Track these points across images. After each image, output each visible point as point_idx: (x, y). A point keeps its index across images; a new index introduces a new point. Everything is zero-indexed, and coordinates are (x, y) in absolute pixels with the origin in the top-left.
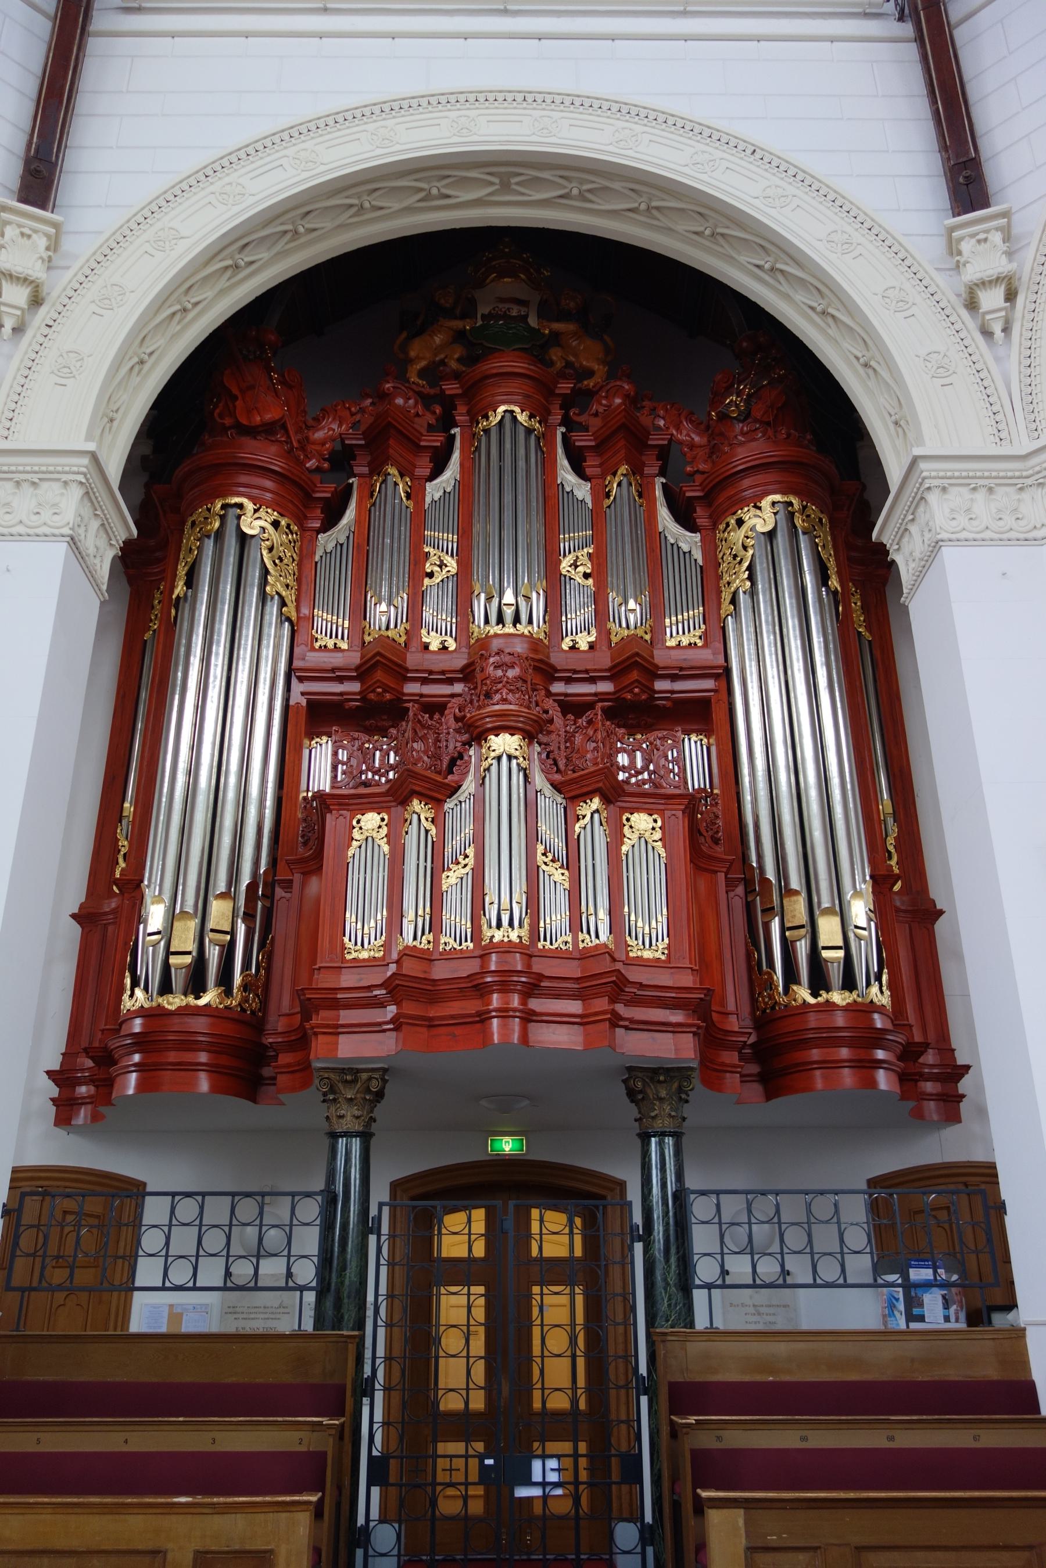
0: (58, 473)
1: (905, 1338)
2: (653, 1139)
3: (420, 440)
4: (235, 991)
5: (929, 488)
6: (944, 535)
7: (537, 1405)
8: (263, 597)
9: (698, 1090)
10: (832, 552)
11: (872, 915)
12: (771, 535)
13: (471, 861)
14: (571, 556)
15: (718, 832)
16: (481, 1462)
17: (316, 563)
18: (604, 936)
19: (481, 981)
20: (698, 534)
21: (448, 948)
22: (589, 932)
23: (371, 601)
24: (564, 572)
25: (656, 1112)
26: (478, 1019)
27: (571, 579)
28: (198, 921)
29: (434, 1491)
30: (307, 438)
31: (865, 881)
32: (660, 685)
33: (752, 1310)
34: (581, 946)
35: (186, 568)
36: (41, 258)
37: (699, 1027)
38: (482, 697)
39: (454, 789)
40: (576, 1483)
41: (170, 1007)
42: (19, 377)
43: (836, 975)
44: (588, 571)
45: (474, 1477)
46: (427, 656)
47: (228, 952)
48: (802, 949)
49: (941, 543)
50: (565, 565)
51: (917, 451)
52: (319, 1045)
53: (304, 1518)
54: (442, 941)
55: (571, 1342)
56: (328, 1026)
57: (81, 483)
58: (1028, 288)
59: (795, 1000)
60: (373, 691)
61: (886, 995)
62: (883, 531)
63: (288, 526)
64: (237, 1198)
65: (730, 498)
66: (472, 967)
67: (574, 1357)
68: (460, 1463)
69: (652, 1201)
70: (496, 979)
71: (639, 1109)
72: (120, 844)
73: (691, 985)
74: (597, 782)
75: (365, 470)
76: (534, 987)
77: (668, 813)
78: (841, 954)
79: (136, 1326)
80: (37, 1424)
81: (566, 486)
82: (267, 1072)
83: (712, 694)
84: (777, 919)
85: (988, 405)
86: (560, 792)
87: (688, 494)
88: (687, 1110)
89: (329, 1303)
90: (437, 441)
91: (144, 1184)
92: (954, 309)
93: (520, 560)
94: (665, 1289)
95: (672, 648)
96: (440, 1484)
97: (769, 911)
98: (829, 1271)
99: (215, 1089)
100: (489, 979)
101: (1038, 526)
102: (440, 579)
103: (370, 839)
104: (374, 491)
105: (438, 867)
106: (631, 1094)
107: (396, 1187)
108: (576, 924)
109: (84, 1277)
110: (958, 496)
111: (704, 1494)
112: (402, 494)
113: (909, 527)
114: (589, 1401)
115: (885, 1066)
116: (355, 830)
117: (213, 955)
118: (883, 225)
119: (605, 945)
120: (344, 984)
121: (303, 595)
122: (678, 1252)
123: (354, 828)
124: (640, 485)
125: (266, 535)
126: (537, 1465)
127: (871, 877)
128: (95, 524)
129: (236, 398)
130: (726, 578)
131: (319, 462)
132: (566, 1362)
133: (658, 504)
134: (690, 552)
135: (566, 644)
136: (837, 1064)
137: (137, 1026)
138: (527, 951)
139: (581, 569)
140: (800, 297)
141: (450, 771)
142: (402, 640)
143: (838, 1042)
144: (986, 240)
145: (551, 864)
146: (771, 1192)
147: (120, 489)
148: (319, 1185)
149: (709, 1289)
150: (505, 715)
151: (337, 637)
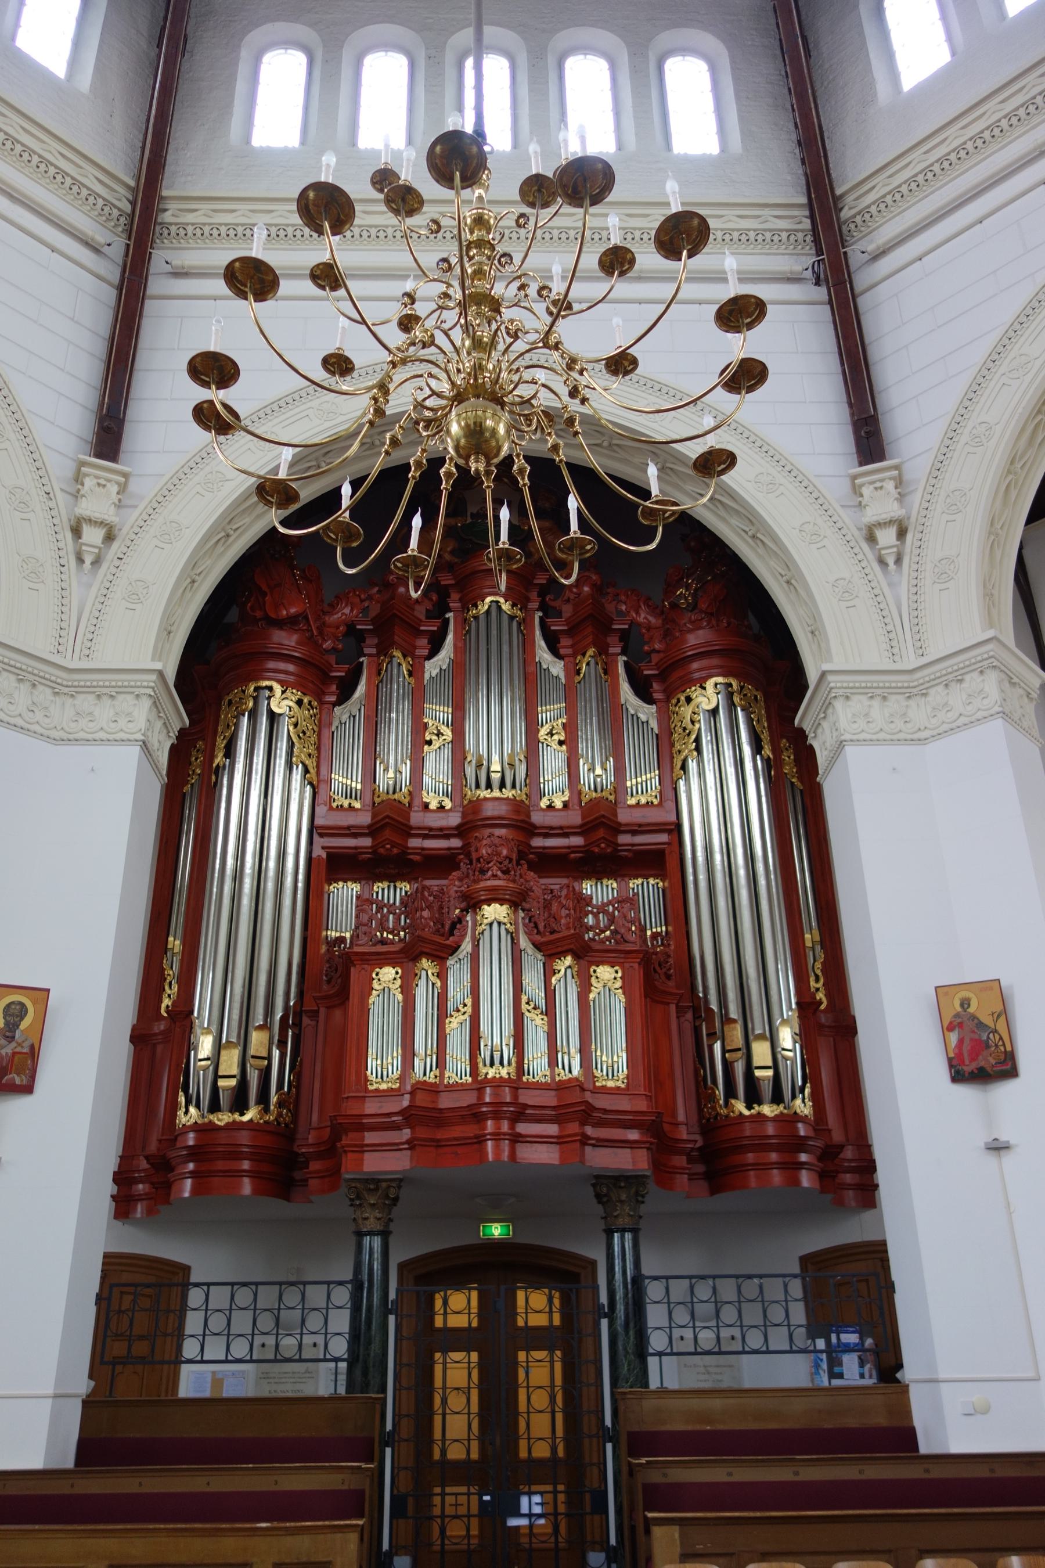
0: (132, 687)
1: (812, 1394)
2: (616, 1234)
3: (420, 626)
4: (272, 1107)
5: (835, 697)
6: (847, 737)
7: (523, 1454)
8: (290, 765)
9: (652, 1187)
10: (766, 725)
11: (797, 1038)
12: (714, 712)
13: (469, 1009)
14: (547, 726)
15: (670, 969)
16: (481, 1498)
17: (333, 733)
18: (576, 1071)
19: (478, 1111)
20: (654, 706)
21: (451, 1082)
22: (563, 1068)
23: (379, 769)
24: (541, 739)
25: (618, 1212)
26: (475, 1140)
27: (548, 746)
28: (240, 1048)
29: (443, 1522)
30: (324, 623)
31: (790, 1008)
32: (624, 839)
33: (702, 1370)
34: (557, 1079)
35: (225, 742)
36: (114, 503)
37: (651, 1143)
38: (477, 873)
39: (454, 949)
40: (556, 1514)
41: (219, 1123)
42: (97, 603)
43: (767, 1090)
44: (562, 738)
45: (474, 1510)
46: (428, 815)
47: (265, 1074)
48: (739, 1068)
49: (844, 743)
50: (543, 732)
51: (826, 667)
52: (348, 1161)
53: (353, 1537)
54: (446, 1076)
55: (551, 1401)
56: (355, 1146)
57: (150, 695)
58: (915, 528)
59: (733, 1112)
60: (383, 847)
61: (808, 1106)
62: (804, 718)
63: (310, 703)
64: (283, 1287)
65: (680, 678)
66: (470, 1099)
67: (553, 1413)
68: (463, 1499)
69: (614, 1285)
70: (490, 1109)
71: (605, 1209)
72: (166, 973)
73: (645, 1109)
74: (571, 944)
75: (374, 651)
76: (520, 1114)
77: (627, 965)
78: (770, 1073)
79: (185, 1391)
80: (138, 1471)
81: (543, 664)
82: (298, 1175)
83: (666, 846)
84: (719, 1042)
85: (883, 625)
86: (540, 950)
87: (646, 672)
88: (643, 1209)
89: (358, 1372)
90: (434, 626)
91: (186, 1269)
92: (857, 542)
93: (504, 681)
94: (625, 1356)
95: (631, 806)
96: (448, 1516)
97: (712, 1035)
98: (755, 1340)
99: (256, 1191)
100: (484, 1109)
101: (922, 728)
102: (438, 745)
103: (386, 989)
104: (381, 670)
105: (443, 1014)
106: (598, 1197)
107: (402, 1267)
108: (553, 1062)
109: (141, 1348)
110: (858, 703)
111: (650, 1515)
112: (405, 672)
113: (821, 722)
114: (567, 1448)
115: (806, 1167)
116: (375, 981)
117: (253, 1077)
118: (801, 469)
119: (576, 1079)
120: (368, 1111)
121: (322, 761)
122: (635, 1327)
123: (373, 979)
124: (606, 663)
125: (291, 713)
126: (524, 1501)
127: (797, 1003)
128: (159, 724)
129: (266, 594)
130: (677, 746)
131: (334, 642)
132: (547, 1417)
133: (621, 679)
134: (647, 722)
135: (544, 803)
136: (767, 1166)
137: (191, 1139)
138: (516, 1083)
139: (556, 737)
140: (734, 521)
141: (452, 934)
142: (406, 801)
143: (770, 1148)
144: (881, 488)
145: (533, 1011)
146: (710, 1277)
147: (175, 686)
148: (349, 1276)
149: (660, 1356)
150: (495, 890)
151: (351, 797)
